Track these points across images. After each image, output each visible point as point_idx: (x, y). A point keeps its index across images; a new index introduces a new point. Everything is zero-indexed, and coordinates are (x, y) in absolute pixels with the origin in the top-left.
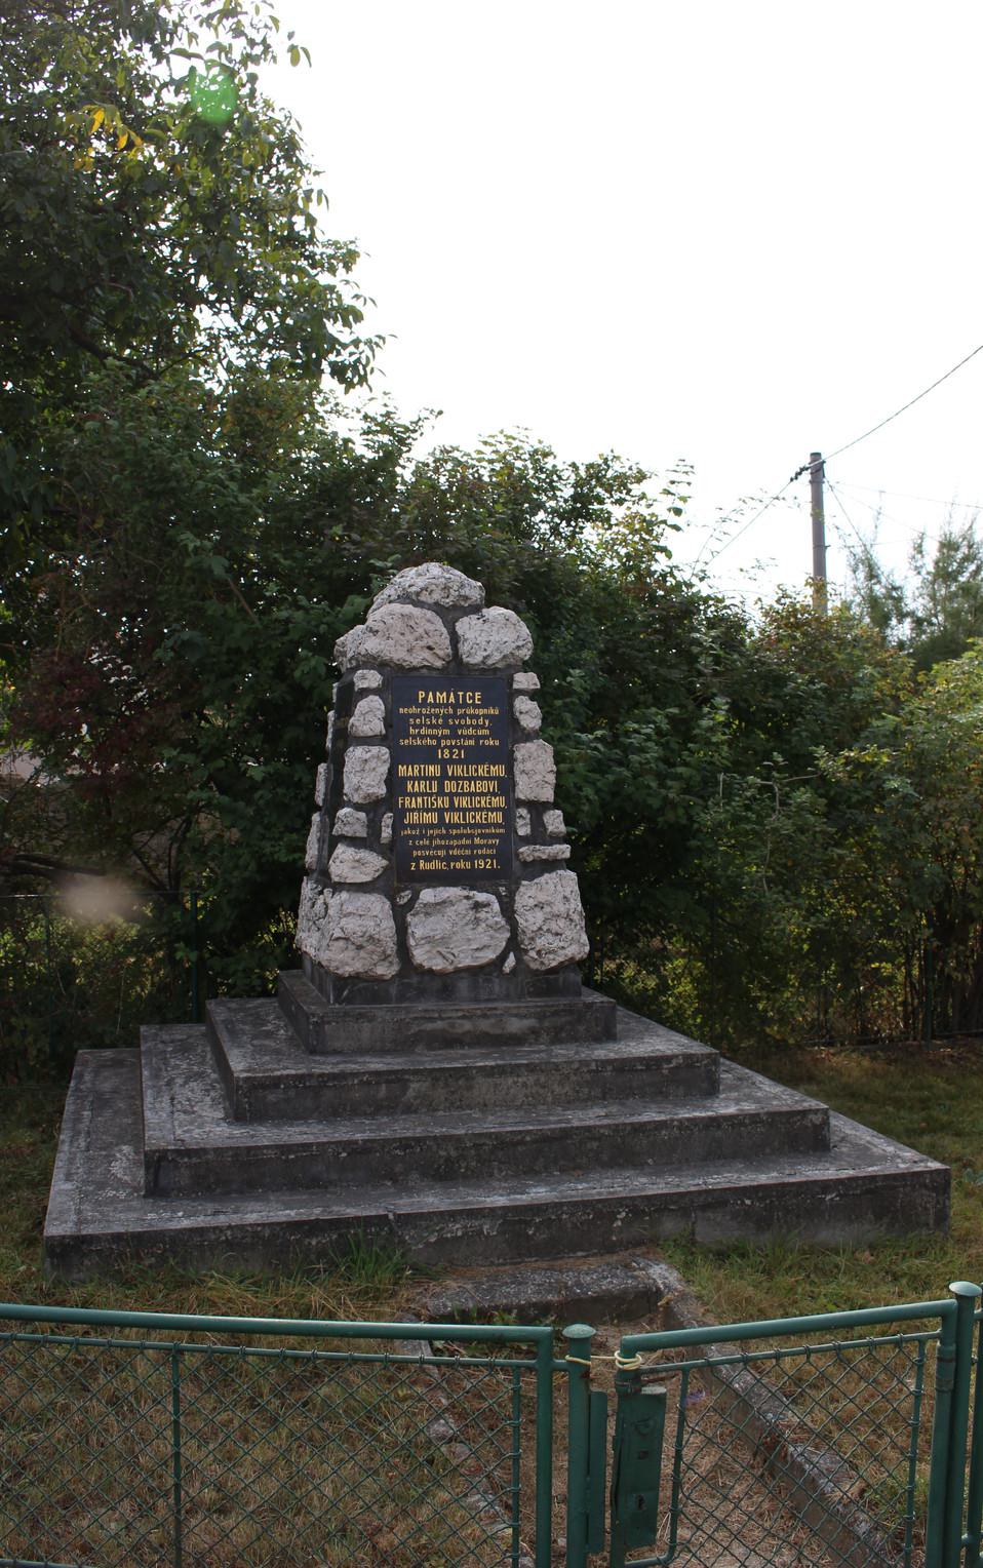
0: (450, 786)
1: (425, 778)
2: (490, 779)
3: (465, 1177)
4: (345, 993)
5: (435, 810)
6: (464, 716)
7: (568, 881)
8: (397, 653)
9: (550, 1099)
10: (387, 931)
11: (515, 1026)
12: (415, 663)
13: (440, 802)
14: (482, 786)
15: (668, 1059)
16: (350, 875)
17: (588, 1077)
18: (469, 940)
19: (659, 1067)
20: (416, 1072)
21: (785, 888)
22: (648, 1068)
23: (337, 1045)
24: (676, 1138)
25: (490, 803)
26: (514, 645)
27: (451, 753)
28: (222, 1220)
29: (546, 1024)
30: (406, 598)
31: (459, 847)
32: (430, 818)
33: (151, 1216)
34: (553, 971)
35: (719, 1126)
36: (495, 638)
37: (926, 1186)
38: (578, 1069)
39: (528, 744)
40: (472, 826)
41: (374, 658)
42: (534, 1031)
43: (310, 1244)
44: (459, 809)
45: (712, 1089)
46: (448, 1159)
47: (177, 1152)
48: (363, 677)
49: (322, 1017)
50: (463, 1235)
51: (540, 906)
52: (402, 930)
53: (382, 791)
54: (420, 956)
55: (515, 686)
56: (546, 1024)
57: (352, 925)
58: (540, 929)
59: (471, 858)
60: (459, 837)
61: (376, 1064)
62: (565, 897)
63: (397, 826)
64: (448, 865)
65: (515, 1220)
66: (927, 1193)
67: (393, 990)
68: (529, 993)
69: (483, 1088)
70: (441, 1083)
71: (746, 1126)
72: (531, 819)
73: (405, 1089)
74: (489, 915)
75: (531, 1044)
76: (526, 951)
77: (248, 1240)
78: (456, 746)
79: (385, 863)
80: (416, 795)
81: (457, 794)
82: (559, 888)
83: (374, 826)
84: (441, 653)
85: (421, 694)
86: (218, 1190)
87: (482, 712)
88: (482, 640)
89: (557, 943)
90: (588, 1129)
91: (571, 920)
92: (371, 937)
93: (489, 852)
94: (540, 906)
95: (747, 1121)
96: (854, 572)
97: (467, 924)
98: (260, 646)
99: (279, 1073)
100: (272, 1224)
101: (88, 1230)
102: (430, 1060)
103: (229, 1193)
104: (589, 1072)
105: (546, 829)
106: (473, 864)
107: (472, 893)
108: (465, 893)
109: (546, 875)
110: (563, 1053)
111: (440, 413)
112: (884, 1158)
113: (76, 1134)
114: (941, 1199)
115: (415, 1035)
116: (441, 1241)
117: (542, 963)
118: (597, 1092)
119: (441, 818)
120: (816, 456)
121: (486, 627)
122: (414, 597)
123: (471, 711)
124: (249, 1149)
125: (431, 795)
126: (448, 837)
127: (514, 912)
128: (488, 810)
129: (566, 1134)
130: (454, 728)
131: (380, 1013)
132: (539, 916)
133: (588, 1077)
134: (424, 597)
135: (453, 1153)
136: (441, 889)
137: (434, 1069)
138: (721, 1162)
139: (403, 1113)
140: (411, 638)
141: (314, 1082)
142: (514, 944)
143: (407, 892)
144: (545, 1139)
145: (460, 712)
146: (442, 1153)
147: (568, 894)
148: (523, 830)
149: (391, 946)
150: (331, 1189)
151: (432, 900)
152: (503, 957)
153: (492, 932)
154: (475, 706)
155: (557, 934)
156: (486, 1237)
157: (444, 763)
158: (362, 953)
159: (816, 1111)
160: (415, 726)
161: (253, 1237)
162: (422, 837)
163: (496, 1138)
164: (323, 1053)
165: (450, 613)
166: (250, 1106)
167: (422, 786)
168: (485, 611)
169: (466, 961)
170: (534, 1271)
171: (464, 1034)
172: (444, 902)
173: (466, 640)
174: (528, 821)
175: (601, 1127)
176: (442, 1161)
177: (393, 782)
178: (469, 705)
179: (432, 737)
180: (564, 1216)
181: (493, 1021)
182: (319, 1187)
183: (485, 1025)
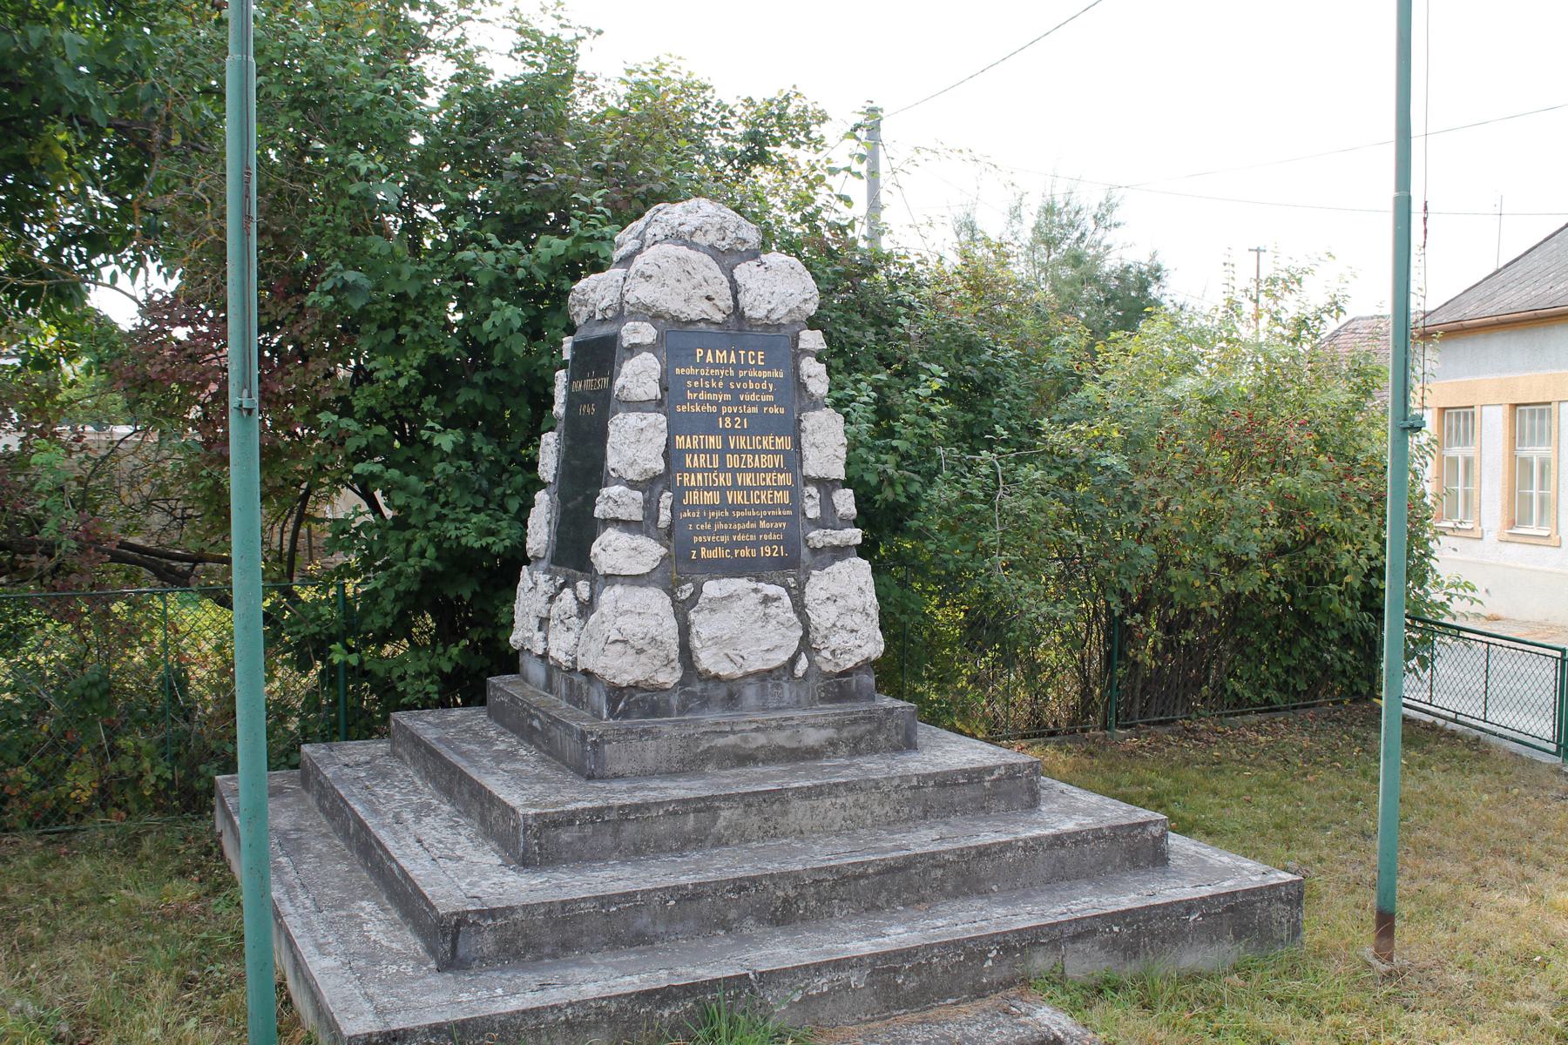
0: (732, 461)
1: (705, 451)
2: (775, 452)
3: (803, 919)
6: (746, 379)
7: (860, 570)
8: (672, 303)
9: (869, 822)
10: (670, 631)
11: (813, 737)
13: (722, 479)
14: (767, 461)
15: (990, 770)
16: (626, 566)
17: (909, 794)
18: (758, 640)
19: (981, 781)
20: (727, 798)
22: (970, 781)
23: (618, 768)
24: (1020, 860)
25: (776, 481)
26: (801, 298)
27: (734, 422)
28: (555, 996)
29: (845, 734)
30: (676, 238)
32: (711, 498)
33: (464, 997)
35: (1063, 845)
37: (1281, 899)
39: (817, 413)
41: (648, 309)
42: (832, 743)
43: (662, 1016)
44: (742, 488)
46: (786, 900)
47: (479, 912)
48: (635, 331)
49: (601, 736)
50: (830, 990)
51: (833, 599)
52: (685, 630)
53: (660, 466)
54: (708, 660)
55: (801, 345)
56: (845, 734)
57: (630, 625)
58: (834, 625)
59: (754, 545)
61: (678, 790)
62: (860, 589)
64: (732, 553)
65: (884, 967)
66: (1282, 906)
67: (675, 701)
68: (821, 698)
69: (799, 812)
71: (1088, 843)
73: (715, 821)
74: (779, 611)
76: (818, 651)
77: (592, 1018)
78: (738, 414)
79: (663, 551)
81: (740, 470)
83: (651, 508)
84: (721, 305)
85: (699, 352)
86: (528, 956)
87: (765, 374)
89: (853, 641)
92: (653, 639)
94: (833, 599)
96: (958, 235)
100: (619, 996)
101: (398, 1023)
103: (541, 958)
104: (911, 788)
105: (835, 511)
106: (758, 552)
107: (761, 585)
108: (753, 585)
109: (838, 564)
110: (875, 766)
111: (600, 32)
112: (1226, 872)
114: (1295, 911)
115: (705, 752)
116: (807, 1000)
117: (837, 664)
118: (918, 811)
119: (724, 498)
120: (873, 112)
121: (769, 275)
122: (687, 238)
123: (752, 373)
124: (564, 903)
125: (712, 470)
129: (910, 862)
131: (666, 729)
133: (909, 794)
135: (792, 893)
136: (725, 580)
137: (746, 794)
138: (1066, 884)
139: (713, 846)
140: (688, 285)
141: (614, 816)
142: (806, 644)
143: (689, 585)
144: (890, 870)
145: (742, 374)
146: (780, 893)
147: (862, 585)
148: (813, 512)
149: (674, 652)
150: (658, 944)
151: (718, 594)
152: (793, 661)
153: (783, 630)
154: (758, 368)
155: (852, 631)
156: (854, 991)
157: (726, 434)
158: (643, 658)
159: (1156, 823)
160: (693, 390)
161: (597, 1015)
162: (703, 520)
163: (837, 872)
164: (602, 778)
165: (728, 257)
166: (541, 846)
167: (702, 461)
168: (763, 257)
170: (909, 1026)
172: (730, 596)
173: (747, 290)
175: (945, 852)
176: (779, 903)
177: (669, 453)
179: (712, 403)
180: (935, 960)
181: (788, 732)
182: (644, 943)
183: (781, 738)
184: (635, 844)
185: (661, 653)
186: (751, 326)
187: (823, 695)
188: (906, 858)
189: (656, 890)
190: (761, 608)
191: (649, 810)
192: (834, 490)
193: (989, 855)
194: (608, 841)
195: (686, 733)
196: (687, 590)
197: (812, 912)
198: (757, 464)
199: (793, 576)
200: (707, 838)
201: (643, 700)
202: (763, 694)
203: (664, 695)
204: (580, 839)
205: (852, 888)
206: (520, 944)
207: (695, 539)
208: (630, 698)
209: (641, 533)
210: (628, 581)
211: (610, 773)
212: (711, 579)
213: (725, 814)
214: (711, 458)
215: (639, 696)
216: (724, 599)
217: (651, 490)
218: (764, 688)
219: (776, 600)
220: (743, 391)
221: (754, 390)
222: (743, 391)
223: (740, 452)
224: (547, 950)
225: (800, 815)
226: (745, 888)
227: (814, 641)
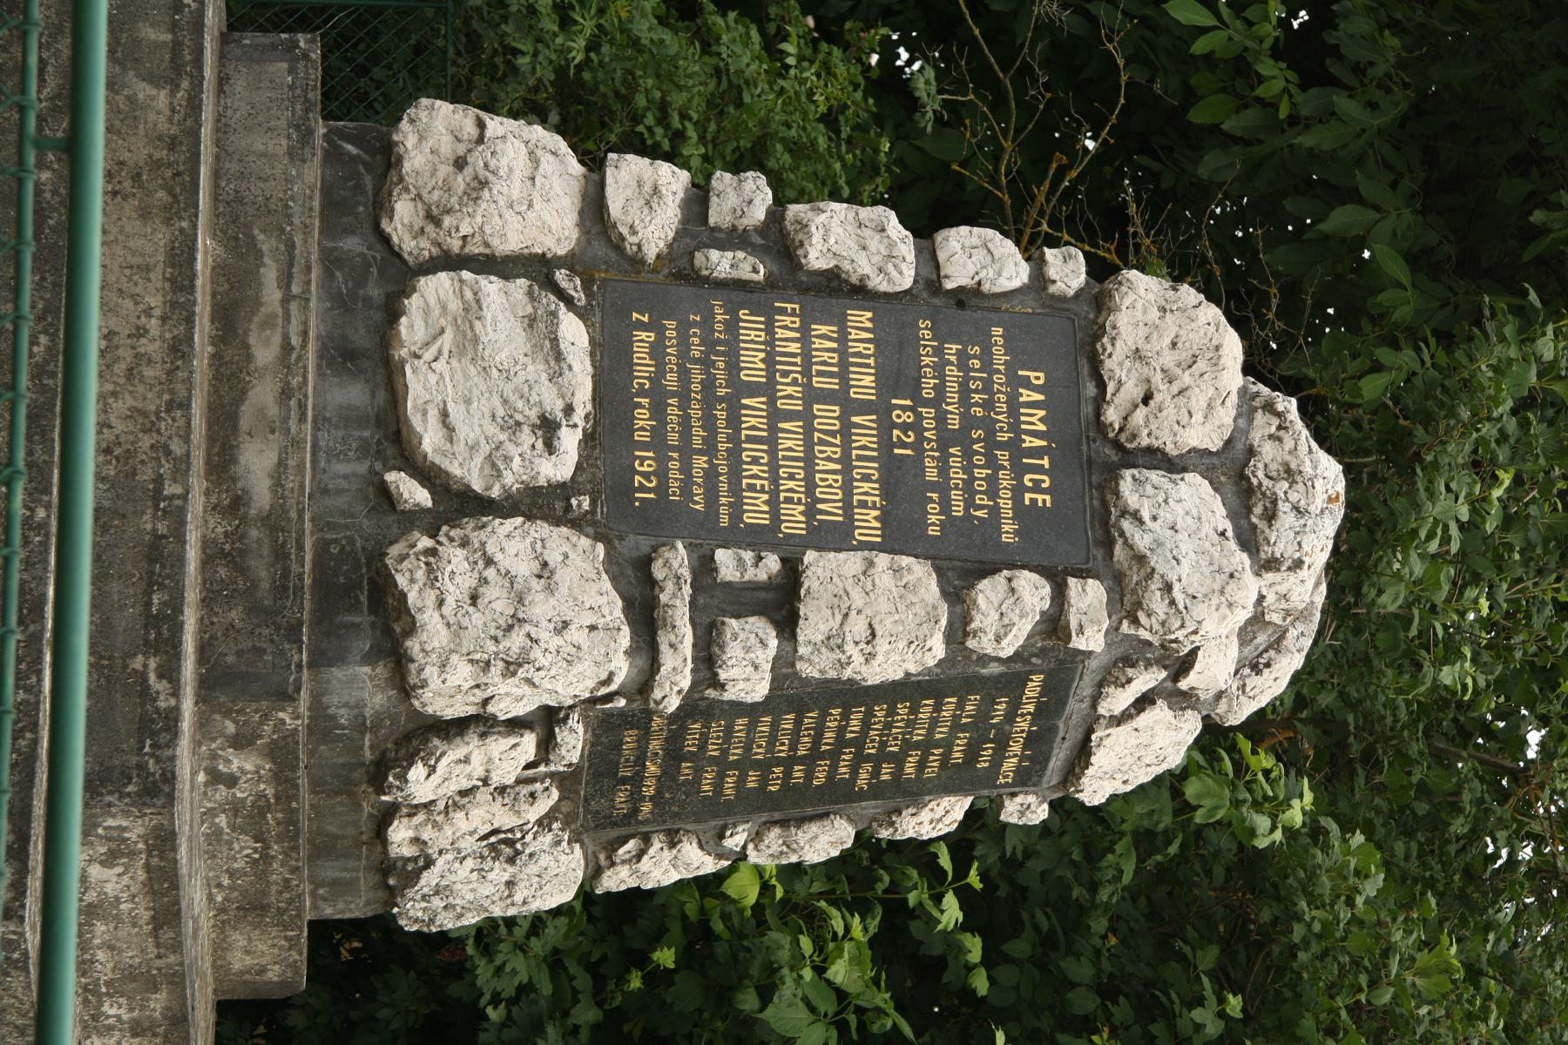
1: (844, 365)
4: (350, 147)
6: (992, 463)
12: (1109, 364)
13: (790, 390)
17: (146, 475)
18: (468, 402)
19: (149, 648)
23: (239, 85)
27: (905, 428)
31: (685, 421)
32: (753, 366)
36: (1186, 546)
38: (168, 452)
40: (735, 455)
44: (773, 429)
53: (816, 258)
54: (437, 288)
58: (489, 562)
59: (658, 441)
60: (709, 423)
62: (566, 624)
64: (642, 392)
67: (352, 244)
70: (162, 154)
73: (151, 79)
74: (526, 447)
75: (207, 493)
78: (920, 439)
81: (809, 430)
82: (588, 619)
83: (733, 239)
85: (1037, 377)
87: (1006, 504)
91: (510, 628)
93: (674, 487)
94: (545, 571)
104: (159, 481)
106: (644, 446)
109: (620, 603)
119: (752, 390)
123: (1005, 480)
125: (806, 372)
126: (709, 400)
127: (530, 517)
128: (774, 493)
132: (524, 568)
133: (146, 475)
145: (1003, 456)
149: (462, 228)
152: (428, 475)
153: (485, 449)
154: (1018, 491)
155: (474, 598)
158: (445, 170)
160: (963, 356)
162: (709, 343)
169: (419, 387)
171: (247, 346)
172: (559, 356)
178: (1019, 478)
179: (940, 389)
181: (273, 411)
183: (263, 395)
185: (454, 200)
186: (1100, 487)
187: (335, 550)
190: (533, 414)
198: (822, 465)
199: (593, 512)
201: (359, 188)
202: (350, 418)
207: (671, 324)
208: (365, 164)
209: (685, 221)
210: (591, 189)
211: (230, 69)
213: (162, 98)
214: (831, 375)
215: (368, 181)
216: (555, 341)
218: (362, 421)
220: (968, 454)
221: (972, 479)
223: (846, 430)
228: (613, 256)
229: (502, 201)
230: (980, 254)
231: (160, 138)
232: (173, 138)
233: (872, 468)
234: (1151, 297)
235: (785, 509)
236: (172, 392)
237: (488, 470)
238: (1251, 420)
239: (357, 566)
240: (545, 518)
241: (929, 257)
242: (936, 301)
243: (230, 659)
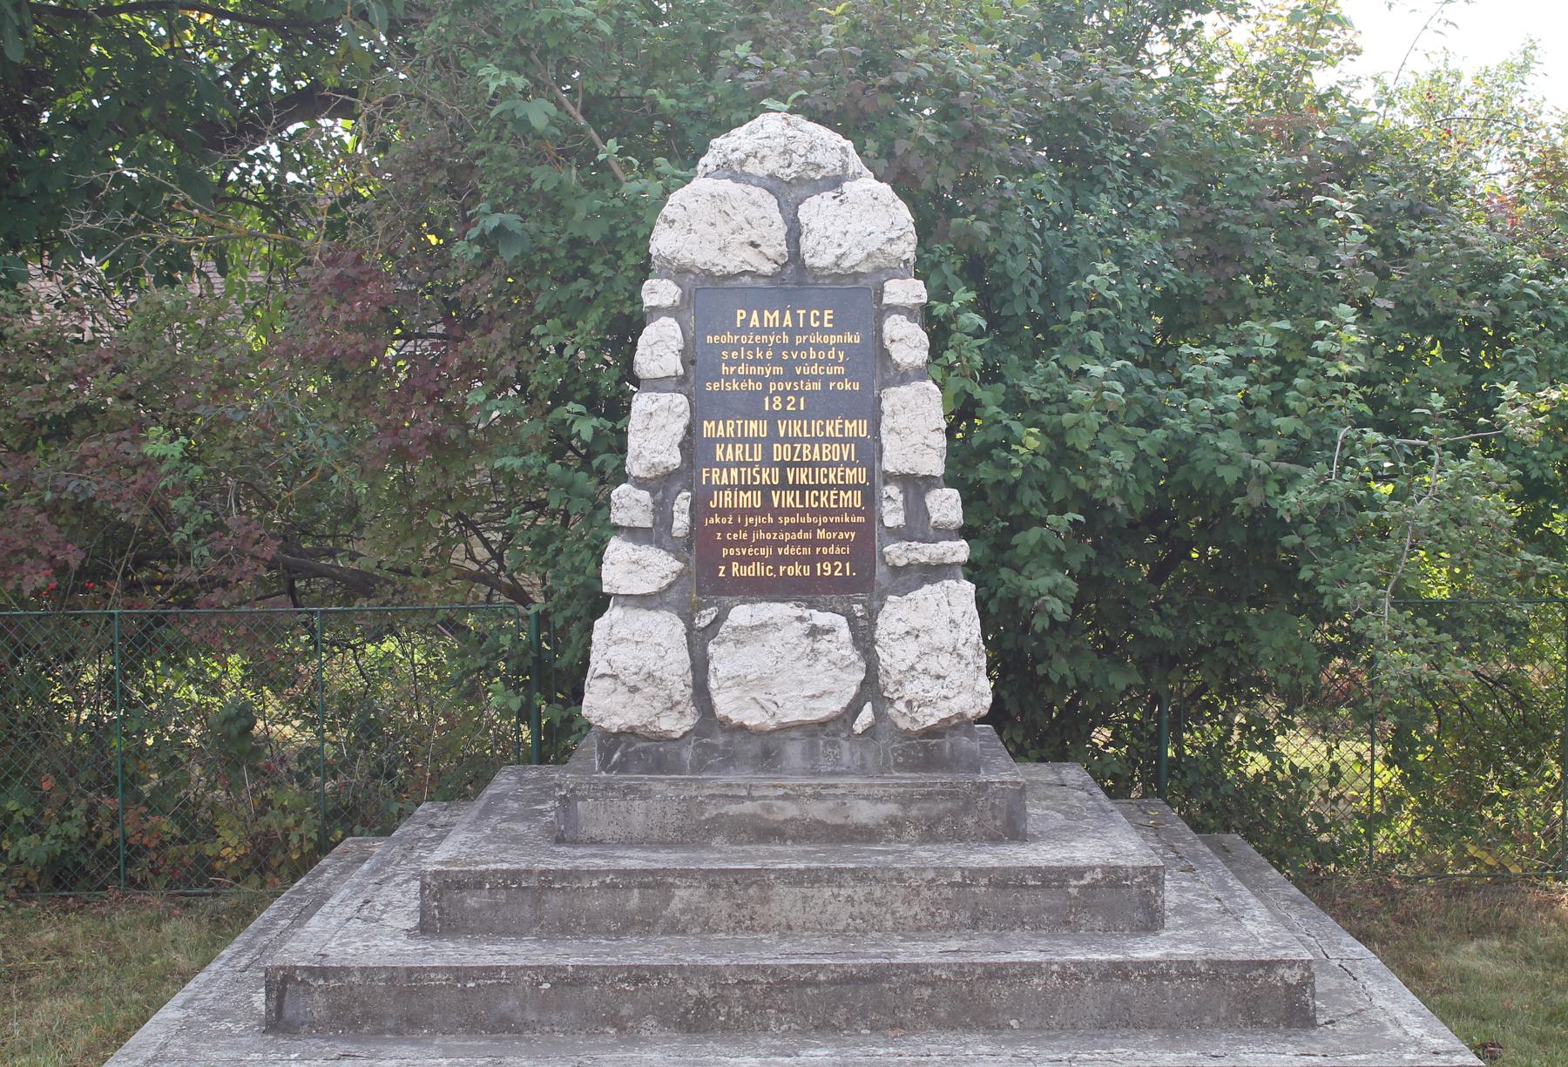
1: (743, 440)
2: (844, 441)
3: (725, 1028)
5: (755, 488)
6: (805, 346)
9: (889, 924)
10: (675, 666)
11: (865, 813)
13: (765, 476)
15: (1079, 872)
17: (949, 893)
18: (801, 682)
19: (1063, 885)
20: (684, 874)
21: (1417, 614)
22: (1046, 884)
23: (595, 831)
24: (1055, 991)
25: (843, 478)
26: (884, 238)
27: (784, 403)
29: (914, 812)
30: (732, 171)
31: (792, 543)
34: (930, 732)
36: (855, 227)
38: (933, 880)
39: (903, 389)
40: (815, 512)
42: (894, 822)
44: (794, 487)
45: (1151, 922)
46: (700, 1001)
48: (653, 291)
49: (572, 791)
52: (700, 666)
53: (674, 459)
54: (726, 704)
55: (886, 300)
56: (914, 812)
58: (912, 668)
59: (811, 560)
60: (795, 528)
61: (634, 860)
62: (952, 621)
63: (699, 510)
64: (776, 570)
67: (688, 754)
69: (785, 900)
71: (1171, 980)
72: (906, 501)
73: (668, 900)
74: (831, 646)
76: (892, 701)
78: (792, 392)
79: (678, 565)
80: (728, 465)
81: (792, 464)
83: (662, 512)
84: (770, 252)
85: (741, 315)
86: (367, 1028)
87: (833, 339)
88: (835, 231)
89: (936, 690)
90: (916, 968)
92: (650, 675)
95: (1173, 971)
97: (798, 659)
98: (619, 234)
99: (483, 867)
102: (720, 856)
103: (382, 1032)
104: (952, 885)
106: (814, 570)
107: (806, 613)
108: (798, 612)
109: (927, 588)
113: (249, 946)
115: (713, 820)
117: (914, 720)
118: (963, 916)
119: (767, 499)
122: (736, 168)
123: (816, 339)
125: (751, 465)
126: (777, 527)
127: (874, 642)
129: (877, 975)
130: (789, 365)
132: (912, 648)
133: (949, 893)
134: (752, 167)
135: (708, 993)
136: (763, 605)
137: (710, 871)
139: (664, 933)
141: (533, 882)
142: (871, 689)
145: (799, 340)
146: (692, 991)
147: (957, 616)
148: (893, 516)
149: (680, 688)
150: (527, 1034)
151: (746, 622)
152: (854, 709)
153: (836, 671)
154: (823, 331)
155: (938, 677)
157: (773, 418)
160: (729, 363)
162: (736, 527)
163: (773, 974)
164: (575, 843)
169: (794, 714)
171: (786, 821)
172: (764, 625)
173: (810, 231)
174: (900, 504)
176: (690, 1004)
177: (691, 443)
178: (815, 330)
179: (755, 378)
181: (830, 804)
182: (510, 1030)
183: (818, 811)
184: (561, 920)
185: (662, 693)
186: (816, 277)
187: (901, 760)
188: (875, 967)
189: (525, 967)
190: (806, 641)
191: (580, 880)
192: (928, 490)
193: (1004, 978)
194: (527, 912)
195: (686, 794)
196: (705, 618)
197: (737, 1021)
198: (816, 456)
199: (862, 602)
200: (656, 922)
201: (645, 751)
202: (811, 753)
203: (673, 746)
204: (490, 906)
205: (795, 998)
206: (357, 1012)
209: (650, 542)
210: (632, 602)
212: (743, 602)
214: (751, 449)
215: (641, 745)
217: (665, 489)
219: (828, 632)
220: (800, 362)
222: (800, 362)
224: (390, 1024)
225: (787, 904)
226: (644, 979)
227: (885, 689)
228: (676, 588)
229: (660, 664)
230: (658, 350)
231: (710, 894)
232: (710, 885)
233: (816, 424)
234: (681, 238)
235: (849, 481)
236: (891, 879)
237: (850, 670)
238: (750, 175)
239: (912, 747)
240: (872, 633)
241: (658, 385)
242: (692, 379)
243: (998, 823)
